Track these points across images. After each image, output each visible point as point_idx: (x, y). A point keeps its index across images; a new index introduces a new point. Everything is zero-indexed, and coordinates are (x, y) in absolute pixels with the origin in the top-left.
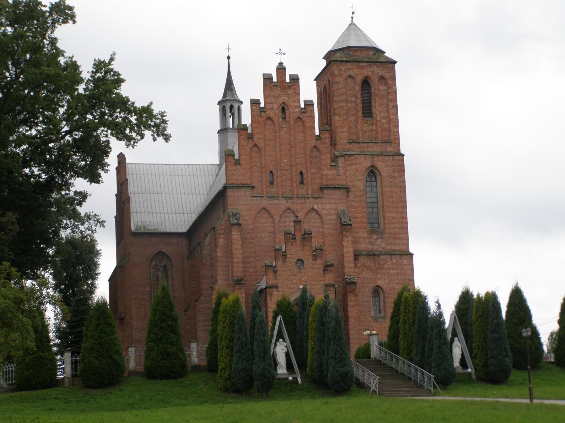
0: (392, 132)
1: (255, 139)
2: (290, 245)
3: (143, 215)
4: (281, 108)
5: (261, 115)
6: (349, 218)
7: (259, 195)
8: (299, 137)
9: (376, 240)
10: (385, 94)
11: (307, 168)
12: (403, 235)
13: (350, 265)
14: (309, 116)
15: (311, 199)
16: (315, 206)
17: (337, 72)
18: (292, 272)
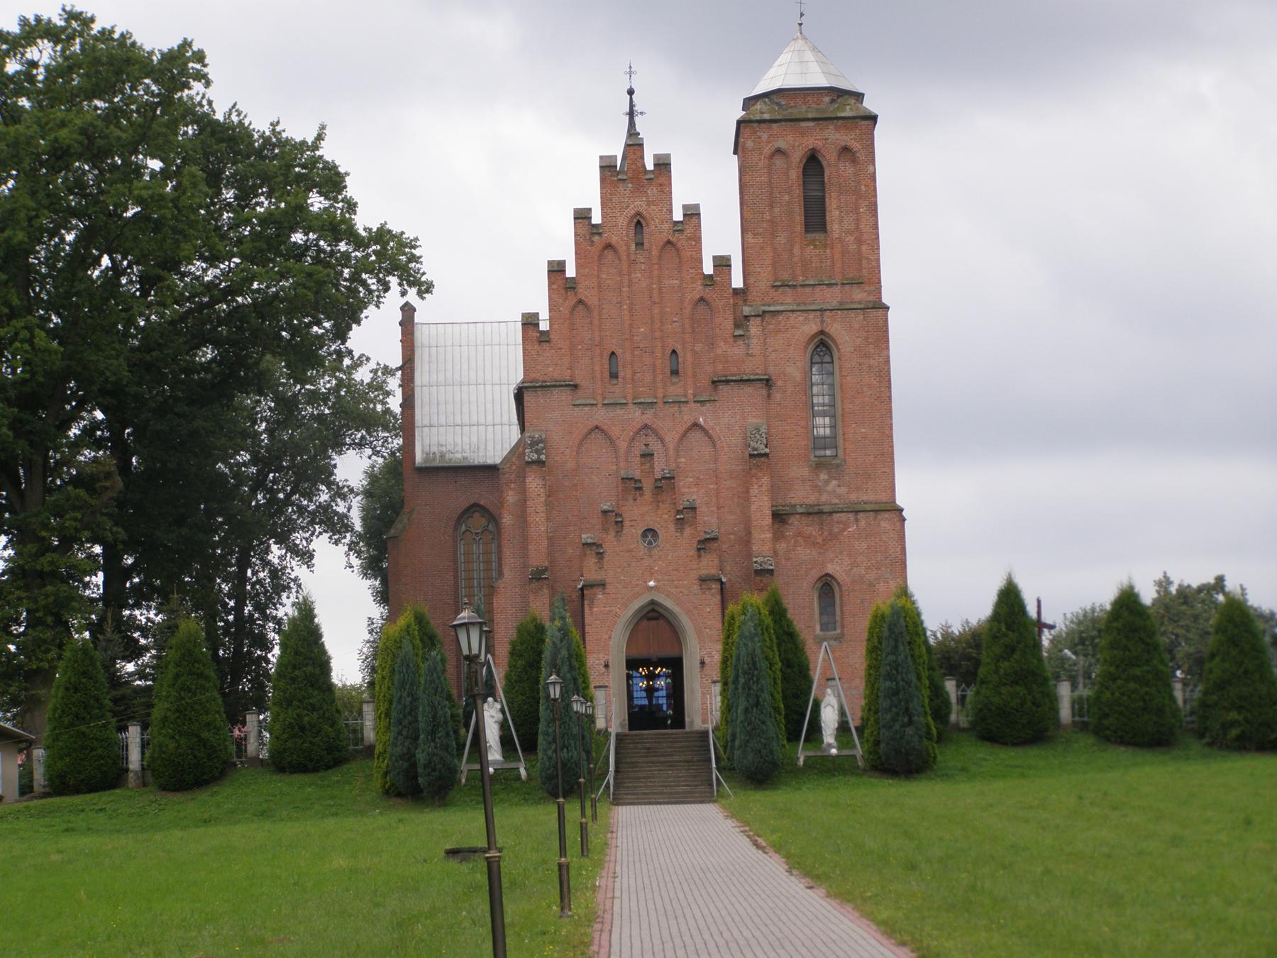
0: (864, 262)
2: (631, 501)
4: (633, 224)
5: (593, 242)
6: (765, 442)
7: (588, 402)
8: (671, 282)
9: (827, 482)
10: (853, 184)
12: (883, 470)
13: (763, 536)
14: (690, 238)
15: (693, 405)
16: (701, 420)
17: (752, 145)
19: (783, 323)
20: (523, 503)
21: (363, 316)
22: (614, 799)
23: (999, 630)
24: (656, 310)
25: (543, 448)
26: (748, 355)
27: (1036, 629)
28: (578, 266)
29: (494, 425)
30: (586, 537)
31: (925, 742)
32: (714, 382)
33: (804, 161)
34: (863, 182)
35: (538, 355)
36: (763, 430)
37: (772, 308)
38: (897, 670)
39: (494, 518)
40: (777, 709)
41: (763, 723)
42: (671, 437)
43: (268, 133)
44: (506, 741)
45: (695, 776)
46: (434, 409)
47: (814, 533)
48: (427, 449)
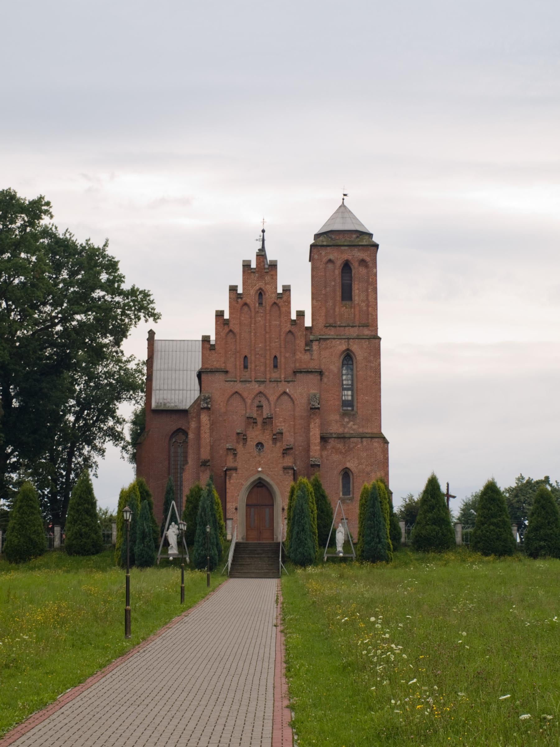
0: (370, 316)
1: (231, 325)
2: (251, 429)
3: (165, 392)
4: (258, 294)
5: (238, 302)
7: (233, 379)
8: (275, 322)
9: (348, 423)
10: (366, 277)
11: (281, 352)
12: (376, 417)
14: (285, 302)
15: (284, 383)
16: (287, 390)
18: (251, 454)
19: (329, 345)
20: (199, 428)
21: (128, 334)
22: (230, 575)
23: (427, 498)
24: (267, 336)
25: (210, 401)
26: (311, 359)
27: (446, 498)
28: (231, 313)
29: (191, 390)
30: (229, 446)
31: (387, 552)
32: (294, 372)
33: (342, 266)
34: (371, 277)
35: (209, 356)
36: (317, 396)
37: (324, 337)
38: (374, 515)
39: (186, 433)
40: (314, 533)
41: (306, 539)
42: (272, 398)
43: (84, 245)
44: (179, 544)
45: (272, 565)
46: (162, 381)
47: (341, 447)
48: (158, 401)
